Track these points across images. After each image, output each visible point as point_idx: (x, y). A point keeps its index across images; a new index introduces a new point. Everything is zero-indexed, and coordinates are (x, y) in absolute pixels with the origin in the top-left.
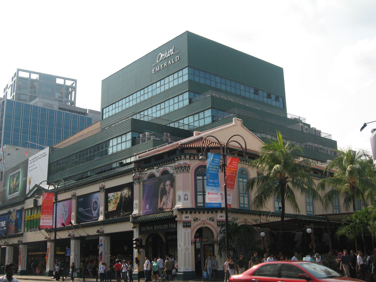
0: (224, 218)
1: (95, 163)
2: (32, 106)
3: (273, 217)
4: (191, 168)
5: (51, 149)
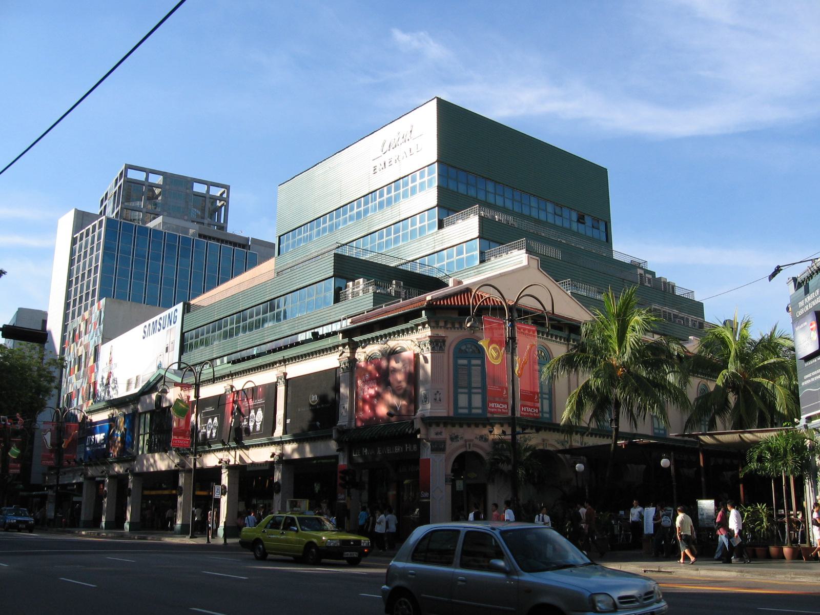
0: (508, 437)
1: (266, 332)
2: (151, 229)
3: (594, 436)
4: (447, 344)
5: (186, 306)
